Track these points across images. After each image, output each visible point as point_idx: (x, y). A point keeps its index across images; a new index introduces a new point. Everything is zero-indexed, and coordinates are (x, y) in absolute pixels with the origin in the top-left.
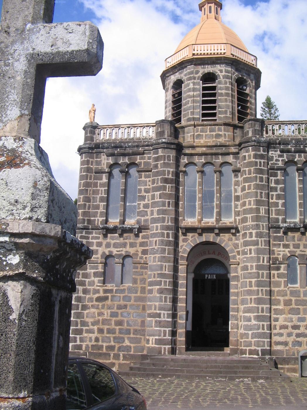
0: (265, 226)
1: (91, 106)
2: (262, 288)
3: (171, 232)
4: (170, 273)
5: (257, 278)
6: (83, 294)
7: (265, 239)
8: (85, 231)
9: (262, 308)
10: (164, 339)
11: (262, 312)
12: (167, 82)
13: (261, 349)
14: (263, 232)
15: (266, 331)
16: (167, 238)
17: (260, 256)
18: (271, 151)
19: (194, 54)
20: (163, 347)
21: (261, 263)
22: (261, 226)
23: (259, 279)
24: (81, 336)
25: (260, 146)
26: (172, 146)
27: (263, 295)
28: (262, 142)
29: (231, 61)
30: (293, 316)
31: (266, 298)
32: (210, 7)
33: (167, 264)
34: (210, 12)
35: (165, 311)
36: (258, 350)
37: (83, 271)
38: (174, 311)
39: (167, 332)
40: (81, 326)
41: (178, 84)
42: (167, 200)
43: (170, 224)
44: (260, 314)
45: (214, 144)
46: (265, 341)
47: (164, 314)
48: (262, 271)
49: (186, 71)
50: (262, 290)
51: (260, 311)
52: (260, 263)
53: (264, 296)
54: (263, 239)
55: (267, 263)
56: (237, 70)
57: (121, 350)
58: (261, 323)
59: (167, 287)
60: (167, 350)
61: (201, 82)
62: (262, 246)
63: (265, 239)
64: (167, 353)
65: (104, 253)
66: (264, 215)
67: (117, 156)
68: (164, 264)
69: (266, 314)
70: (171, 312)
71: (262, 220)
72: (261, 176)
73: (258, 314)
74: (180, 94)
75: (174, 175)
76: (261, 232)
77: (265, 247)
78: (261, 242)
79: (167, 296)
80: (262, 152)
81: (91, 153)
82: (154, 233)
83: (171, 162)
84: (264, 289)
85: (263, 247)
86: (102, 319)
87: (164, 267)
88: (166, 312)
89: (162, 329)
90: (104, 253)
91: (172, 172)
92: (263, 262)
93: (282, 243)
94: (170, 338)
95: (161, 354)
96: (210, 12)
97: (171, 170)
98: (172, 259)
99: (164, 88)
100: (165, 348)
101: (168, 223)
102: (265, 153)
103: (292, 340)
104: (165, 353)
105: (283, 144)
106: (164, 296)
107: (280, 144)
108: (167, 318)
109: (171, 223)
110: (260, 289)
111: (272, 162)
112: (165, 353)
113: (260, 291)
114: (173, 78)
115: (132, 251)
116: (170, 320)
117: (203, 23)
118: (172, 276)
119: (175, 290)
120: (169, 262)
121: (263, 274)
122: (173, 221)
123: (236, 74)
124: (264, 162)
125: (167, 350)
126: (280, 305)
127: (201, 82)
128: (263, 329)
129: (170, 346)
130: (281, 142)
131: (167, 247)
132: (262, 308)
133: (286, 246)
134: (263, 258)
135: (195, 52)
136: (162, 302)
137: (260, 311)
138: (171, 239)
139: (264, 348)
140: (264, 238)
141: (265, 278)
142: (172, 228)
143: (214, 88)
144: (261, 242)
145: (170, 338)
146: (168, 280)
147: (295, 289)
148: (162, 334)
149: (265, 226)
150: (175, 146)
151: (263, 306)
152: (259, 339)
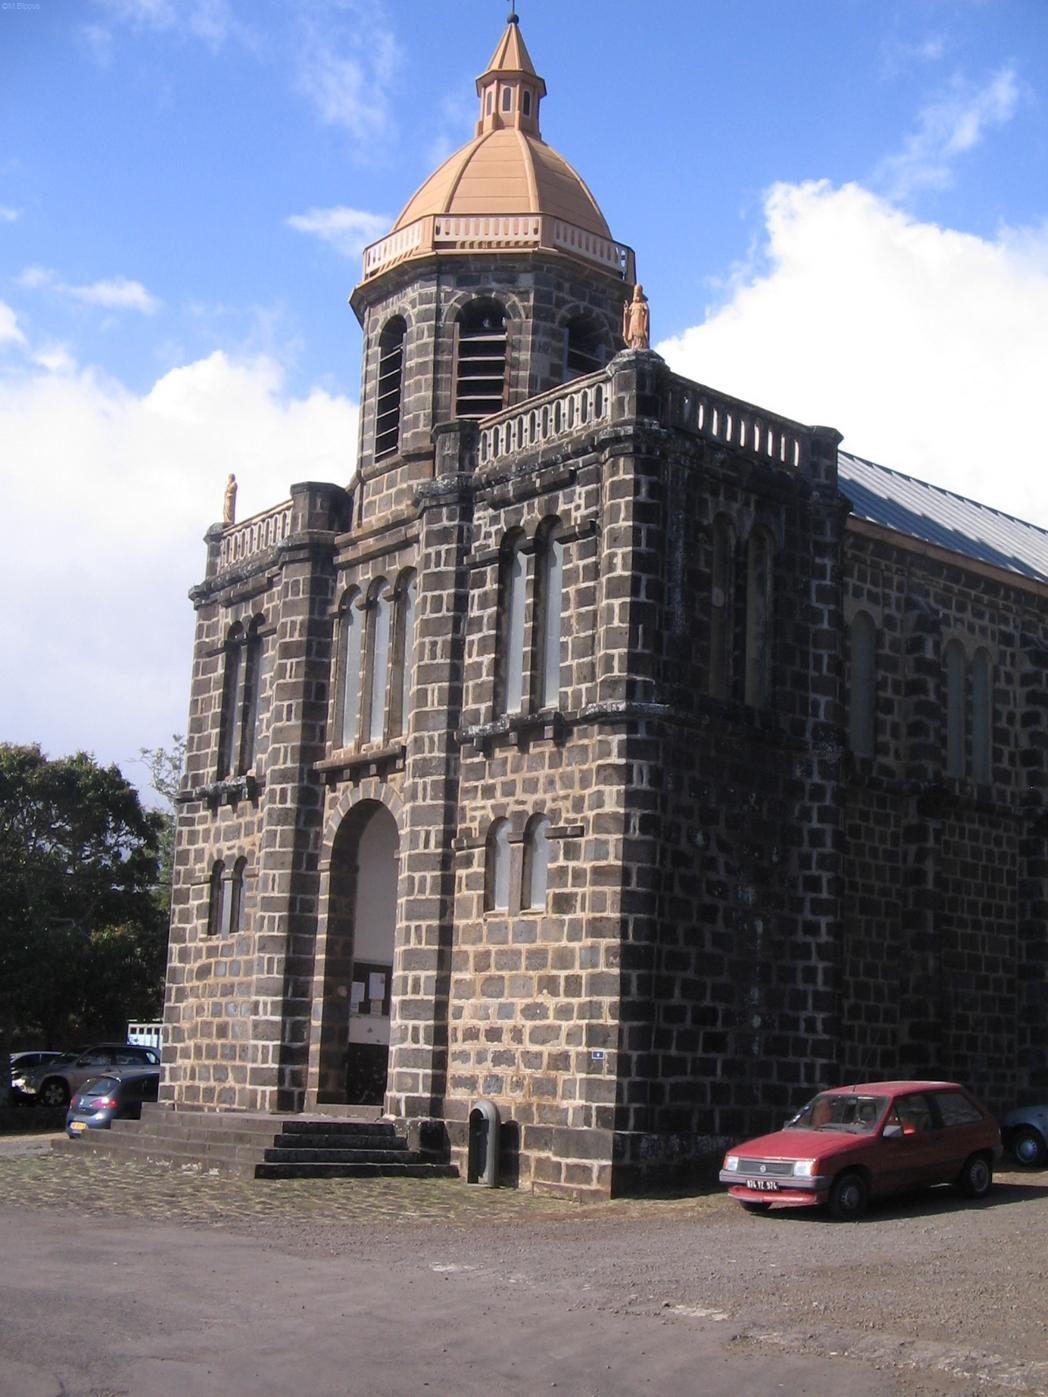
0: (436, 739)
1: (228, 481)
2: (418, 923)
3: (289, 786)
4: (284, 895)
5: (409, 895)
6: (180, 962)
7: (435, 778)
9: (416, 981)
10: (263, 1069)
11: (416, 990)
13: (407, 1098)
14: (431, 759)
15: (423, 1046)
16: (281, 803)
17: (419, 828)
18: (478, 511)
19: (436, 245)
20: (261, 1088)
21: (421, 850)
22: (427, 740)
23: (412, 898)
24: (173, 1065)
25: (440, 506)
26: (302, 554)
27: (420, 943)
28: (440, 492)
29: (433, 264)
30: (490, 1001)
31: (429, 950)
33: (277, 872)
35: (268, 995)
36: (399, 1101)
37: (182, 906)
38: (294, 995)
39: (271, 1049)
40: (174, 1042)
41: (396, 329)
42: (286, 703)
43: (289, 764)
44: (409, 997)
45: (382, 524)
46: (418, 1075)
47: (265, 1004)
48: (422, 873)
50: (418, 928)
51: (409, 989)
52: (417, 851)
53: (423, 946)
54: (429, 779)
55: (436, 847)
56: (461, 282)
57: (223, 1098)
58: (411, 1023)
59: (275, 933)
60: (267, 1099)
61: (458, 324)
62: (424, 799)
63: (435, 778)
64: (267, 1105)
65: (544, 802)
66: (436, 707)
67: (237, 603)
68: (271, 872)
69: (426, 998)
70: (280, 998)
71: (431, 724)
72: (437, 593)
73: (405, 998)
75: (305, 632)
76: (424, 759)
77: (435, 802)
78: (425, 789)
79: (273, 955)
80: (446, 523)
81: (207, 605)
83: (301, 596)
84: (424, 924)
85: (429, 802)
87: (270, 883)
88: (269, 999)
89: (261, 1043)
90: (544, 802)
91: (301, 623)
92: (426, 846)
93: (479, 783)
94: (276, 1066)
95: (255, 1106)
97: (299, 618)
98: (289, 858)
100: (264, 1092)
101: (284, 763)
102: (453, 523)
103: (485, 1073)
104: (263, 1105)
105: (497, 483)
106: (268, 956)
107: (489, 484)
108: (272, 1014)
109: (293, 761)
110: (413, 924)
111: (477, 544)
112: (263, 1105)
113: (413, 930)
114: (382, 314)
116: (278, 1018)
117: (480, 140)
118: (286, 904)
119: (296, 939)
120: (282, 865)
121: (423, 880)
122: (297, 757)
123: (460, 293)
124: (448, 551)
125: (267, 1099)
126: (467, 970)
127: (458, 324)
128: (416, 1040)
129: (276, 1088)
130: (491, 478)
131: (279, 828)
132: (416, 981)
133: (489, 792)
134: (428, 834)
135: (441, 238)
136: (262, 973)
137: (409, 989)
138: (289, 805)
139: (416, 1095)
140: (431, 774)
141: (428, 892)
142: (293, 775)
144: (425, 789)
145: (276, 1066)
146: (277, 915)
147: (497, 920)
149: (436, 739)
150: (306, 551)
151: (418, 973)
152: (404, 1070)
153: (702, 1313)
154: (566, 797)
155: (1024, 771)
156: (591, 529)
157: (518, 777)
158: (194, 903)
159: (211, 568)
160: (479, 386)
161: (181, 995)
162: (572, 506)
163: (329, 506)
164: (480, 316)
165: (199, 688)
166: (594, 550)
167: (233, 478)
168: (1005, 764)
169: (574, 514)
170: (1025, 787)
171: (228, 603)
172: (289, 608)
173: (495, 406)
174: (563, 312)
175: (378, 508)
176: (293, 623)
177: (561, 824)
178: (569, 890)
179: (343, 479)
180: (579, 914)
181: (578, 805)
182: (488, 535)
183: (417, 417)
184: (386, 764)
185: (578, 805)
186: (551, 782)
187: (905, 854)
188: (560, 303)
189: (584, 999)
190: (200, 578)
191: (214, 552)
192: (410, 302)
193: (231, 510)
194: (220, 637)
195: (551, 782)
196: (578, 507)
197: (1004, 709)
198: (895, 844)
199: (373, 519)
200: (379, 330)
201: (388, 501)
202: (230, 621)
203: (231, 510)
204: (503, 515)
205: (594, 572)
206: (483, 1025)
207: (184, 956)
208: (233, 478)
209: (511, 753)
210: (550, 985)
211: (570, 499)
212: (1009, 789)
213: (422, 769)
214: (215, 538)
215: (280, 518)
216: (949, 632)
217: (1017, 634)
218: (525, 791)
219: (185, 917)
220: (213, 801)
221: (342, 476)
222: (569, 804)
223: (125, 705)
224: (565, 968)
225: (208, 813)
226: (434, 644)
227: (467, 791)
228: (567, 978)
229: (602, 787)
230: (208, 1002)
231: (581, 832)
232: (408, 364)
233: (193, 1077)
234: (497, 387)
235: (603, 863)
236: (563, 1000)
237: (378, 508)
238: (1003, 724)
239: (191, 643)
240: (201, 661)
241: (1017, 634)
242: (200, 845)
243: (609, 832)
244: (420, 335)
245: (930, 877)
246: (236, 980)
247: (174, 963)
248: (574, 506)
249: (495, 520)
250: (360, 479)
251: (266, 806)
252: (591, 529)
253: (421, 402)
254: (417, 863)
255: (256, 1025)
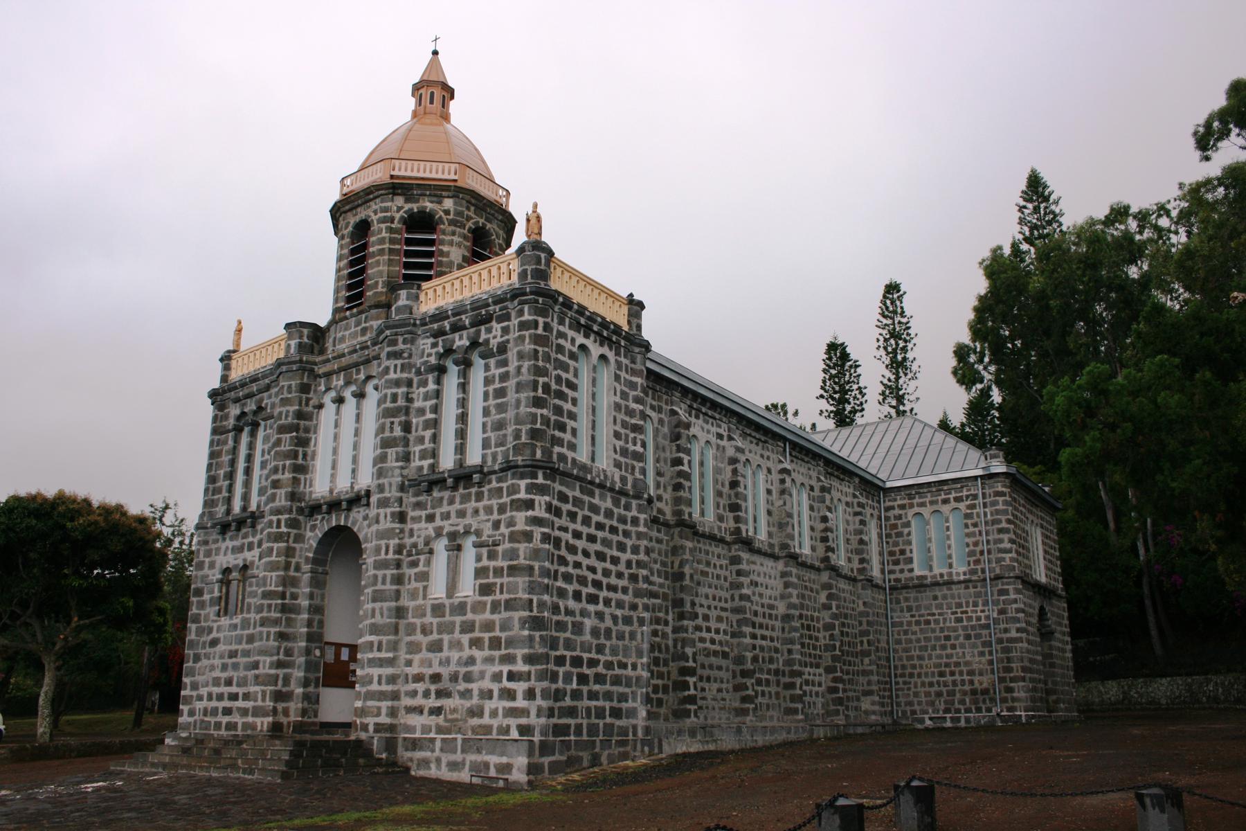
8: (509, 473)
12: (342, 223)
19: (392, 177)
21: (383, 556)
32: (432, 94)
34: (432, 102)
41: (363, 228)
49: (374, 206)
50: (381, 608)
74: (364, 247)
82: (519, 500)
86: (490, 638)
92: (387, 553)
96: (432, 102)
99: (336, 234)
114: (353, 220)
115: (473, 523)
133: (430, 518)
135: (396, 173)
143: (431, 243)
148: (280, 682)
153: (297, 822)
154: (488, 520)
155: (731, 515)
156: (502, 349)
157: (480, 505)
158: (206, 597)
159: (224, 379)
160: (419, 267)
161: (197, 658)
162: (491, 336)
163: (311, 338)
164: (421, 223)
165: (213, 455)
166: (504, 363)
167: (240, 322)
168: (721, 511)
169: (492, 341)
170: (732, 524)
171: (237, 400)
172: (285, 402)
173: (429, 278)
174: (470, 224)
175: (345, 341)
176: (288, 412)
177: (484, 538)
178: (491, 580)
179: (323, 323)
180: (498, 596)
181: (496, 525)
182: (429, 355)
183: (377, 283)
184: (358, 500)
185: (496, 525)
186: (476, 512)
187: (672, 563)
188: (469, 218)
189: (503, 652)
190: (216, 384)
191: (227, 368)
192: (372, 212)
193: (237, 342)
194: (231, 422)
195: (476, 512)
196: (495, 337)
197: (720, 478)
198: (666, 556)
199: (344, 346)
200: (350, 228)
201: (354, 335)
202: (238, 412)
203: (237, 342)
204: (441, 343)
205: (504, 377)
206: (428, 672)
207: (200, 631)
208: (240, 322)
209: (446, 494)
210: (476, 643)
211: (489, 331)
212: (723, 525)
213: (383, 503)
214: (226, 359)
215: (276, 346)
216: (693, 431)
217: (725, 434)
218: (458, 517)
219: (202, 605)
220: (224, 528)
221: (322, 318)
222: (490, 524)
223: (156, 470)
224: (489, 631)
225: (220, 537)
226: (392, 423)
227: (413, 519)
228: (490, 638)
229: (514, 513)
230: (217, 662)
231: (496, 544)
232: (371, 250)
233: (205, 715)
234: (429, 266)
235: (515, 563)
236: (487, 653)
237: (345, 341)
238: (719, 487)
239: (208, 426)
240: (217, 437)
241: (725, 434)
242: (213, 558)
243: (519, 542)
244: (380, 231)
245: (688, 577)
246: (240, 647)
247: (192, 636)
248: (494, 335)
249: (434, 345)
250: (333, 322)
251: (264, 529)
252: (502, 349)
253: (380, 273)
254: (380, 565)
255: (257, 677)
